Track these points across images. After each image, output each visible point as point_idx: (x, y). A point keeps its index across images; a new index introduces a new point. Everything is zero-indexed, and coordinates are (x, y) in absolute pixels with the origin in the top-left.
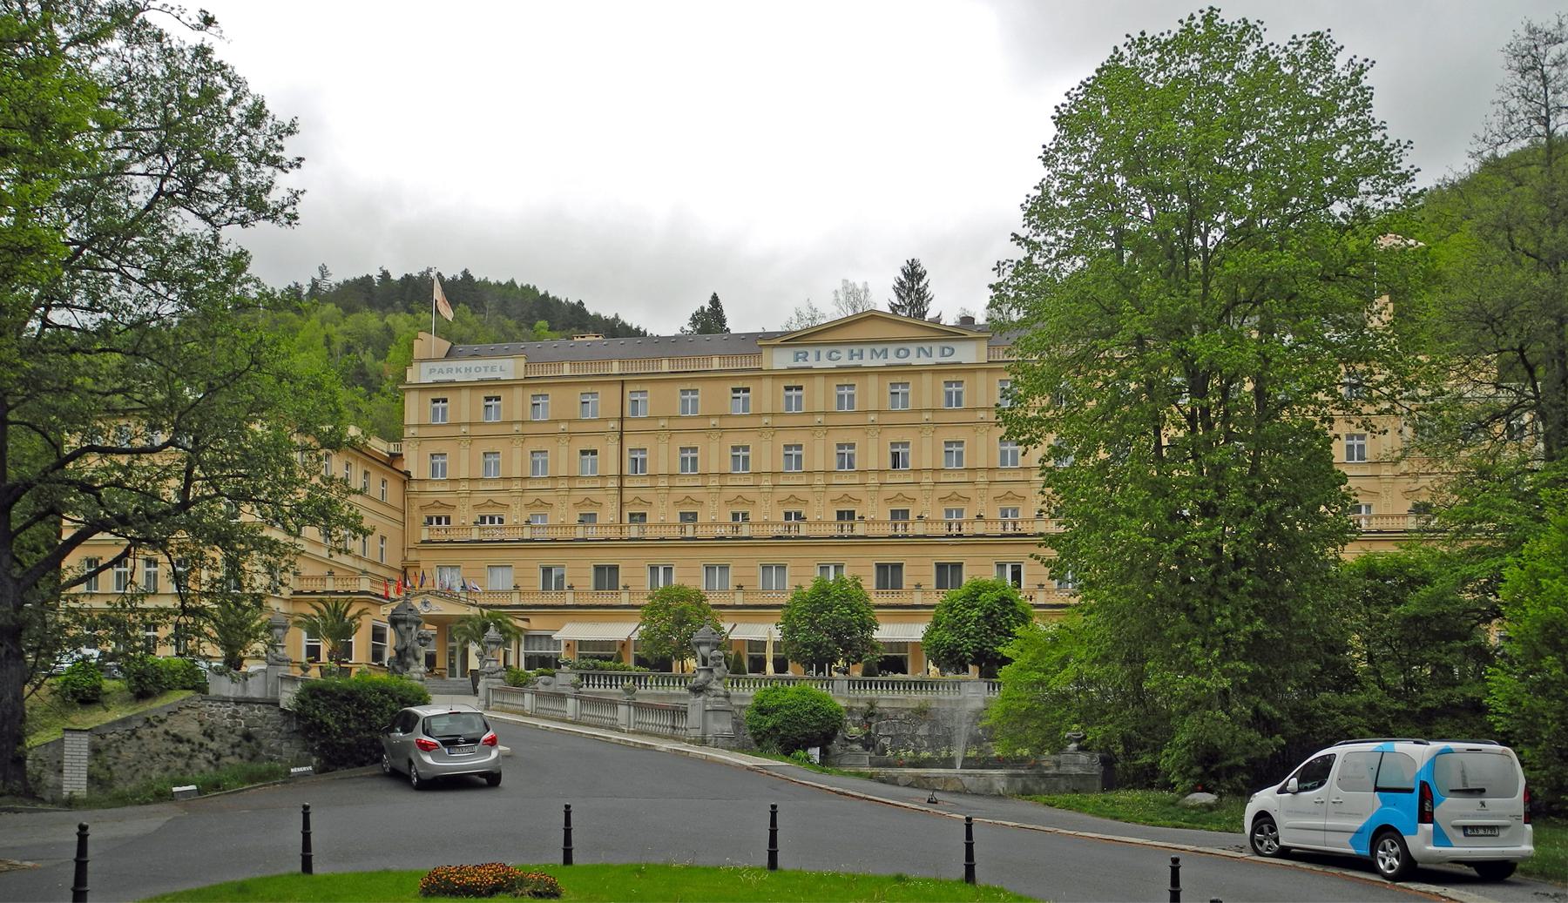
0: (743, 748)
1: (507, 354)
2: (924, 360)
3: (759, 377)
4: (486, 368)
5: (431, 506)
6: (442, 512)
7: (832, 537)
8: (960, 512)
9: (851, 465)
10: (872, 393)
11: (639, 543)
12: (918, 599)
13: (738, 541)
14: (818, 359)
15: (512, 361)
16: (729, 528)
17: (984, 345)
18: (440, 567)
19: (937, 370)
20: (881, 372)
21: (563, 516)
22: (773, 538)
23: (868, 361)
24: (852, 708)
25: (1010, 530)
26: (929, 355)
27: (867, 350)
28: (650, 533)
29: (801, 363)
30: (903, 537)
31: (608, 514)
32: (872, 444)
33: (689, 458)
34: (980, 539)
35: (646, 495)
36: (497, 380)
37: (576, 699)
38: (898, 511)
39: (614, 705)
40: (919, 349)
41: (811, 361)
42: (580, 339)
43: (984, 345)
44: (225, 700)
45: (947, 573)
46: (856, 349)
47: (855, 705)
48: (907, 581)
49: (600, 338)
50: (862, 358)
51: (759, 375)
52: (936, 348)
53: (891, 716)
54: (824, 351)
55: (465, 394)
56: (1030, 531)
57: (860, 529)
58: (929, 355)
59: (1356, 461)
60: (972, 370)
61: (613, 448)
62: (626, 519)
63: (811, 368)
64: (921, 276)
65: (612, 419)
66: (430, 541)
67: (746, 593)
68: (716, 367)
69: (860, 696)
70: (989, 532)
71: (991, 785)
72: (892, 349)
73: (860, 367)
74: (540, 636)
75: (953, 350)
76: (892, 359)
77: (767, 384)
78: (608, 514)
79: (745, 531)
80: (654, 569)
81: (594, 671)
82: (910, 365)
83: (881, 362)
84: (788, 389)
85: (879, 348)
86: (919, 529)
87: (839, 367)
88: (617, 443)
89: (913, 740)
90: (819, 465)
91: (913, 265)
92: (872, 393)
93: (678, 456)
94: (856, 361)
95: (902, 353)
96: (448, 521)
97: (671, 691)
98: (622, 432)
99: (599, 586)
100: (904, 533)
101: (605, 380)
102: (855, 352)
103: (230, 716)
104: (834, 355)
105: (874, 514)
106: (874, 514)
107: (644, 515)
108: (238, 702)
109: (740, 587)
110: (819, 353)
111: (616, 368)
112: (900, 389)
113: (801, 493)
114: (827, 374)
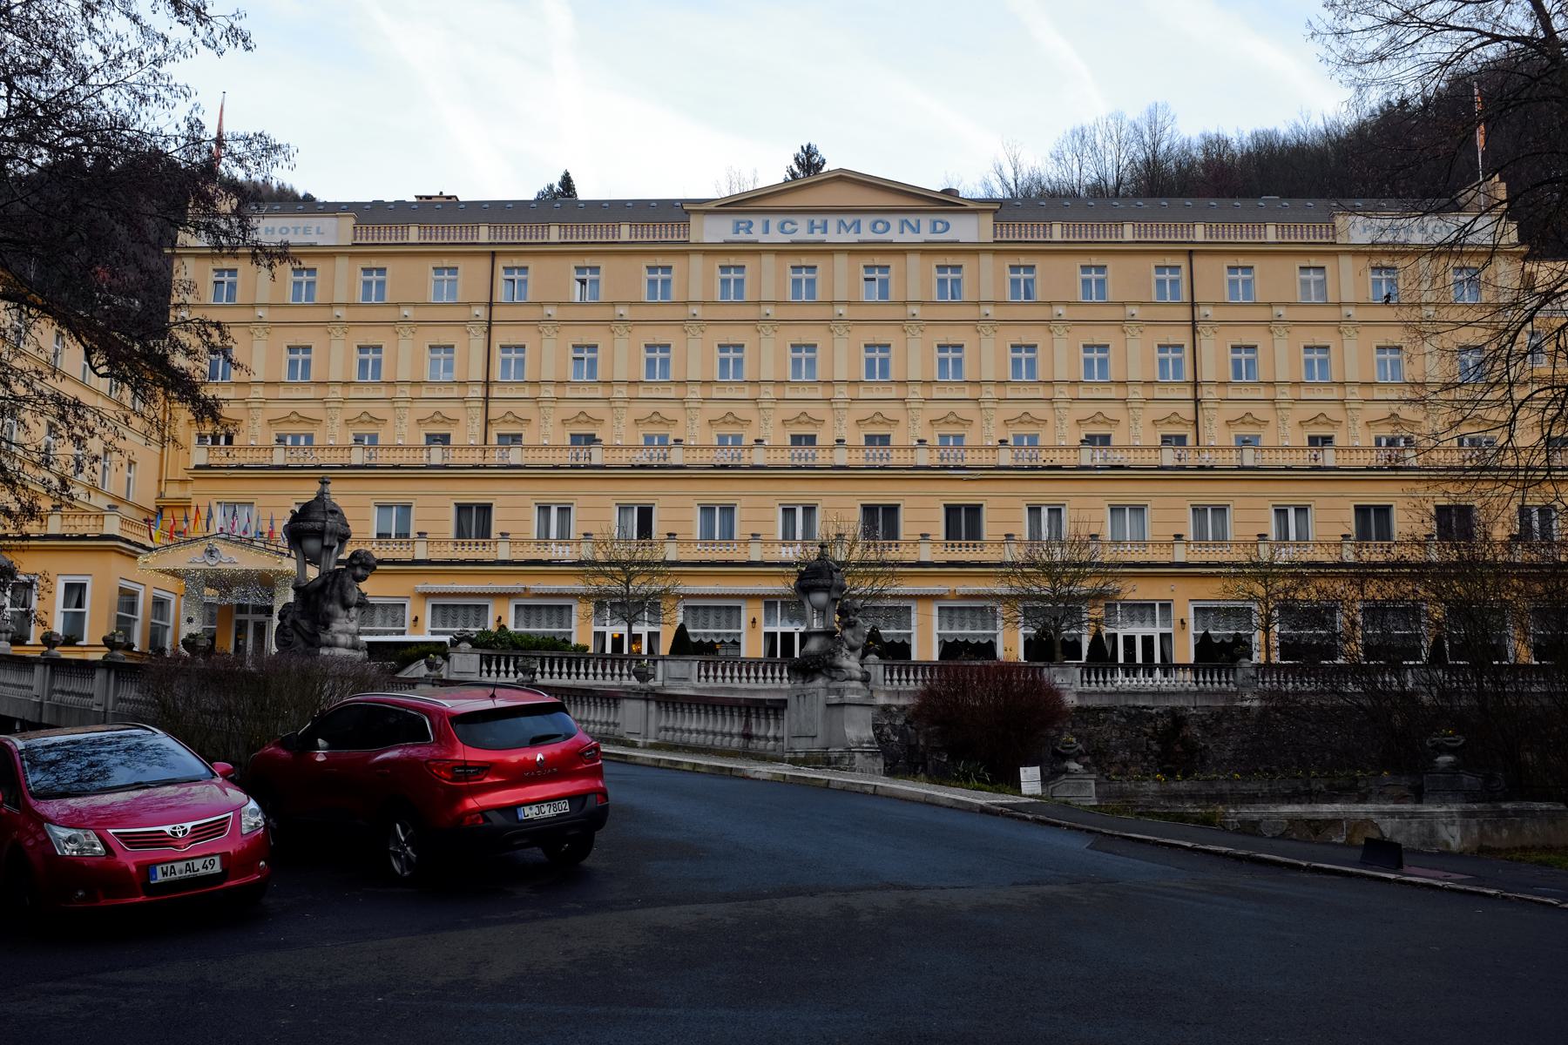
0: (891, 771)
3: (686, 253)
4: (296, 229)
5: (287, 420)
11: (445, 472)
12: (756, 553)
13: (1318, 473)
14: (767, 232)
15: (334, 220)
16: (479, 453)
20: (853, 250)
23: (833, 236)
24: (890, 706)
26: (917, 230)
27: (833, 221)
29: (743, 236)
31: (467, 432)
32: (549, 346)
33: (878, 355)
34: (758, 472)
35: (522, 409)
36: (311, 246)
37: (647, 700)
38: (875, 436)
39: (610, 699)
40: (902, 223)
41: (757, 234)
46: (818, 220)
47: (894, 701)
48: (906, 529)
51: (686, 250)
52: (925, 221)
54: (775, 221)
55: (768, 261)
57: (598, 457)
58: (917, 230)
59: (220, 380)
60: (974, 251)
61: (478, 344)
62: (493, 440)
63: (756, 243)
65: (478, 304)
66: (208, 467)
69: (901, 689)
71: (1433, 832)
72: (866, 221)
73: (823, 243)
75: (948, 224)
76: (867, 234)
77: (696, 262)
78: (467, 432)
79: (1329, 458)
80: (544, 509)
81: (555, 654)
82: (891, 243)
83: (851, 237)
85: (848, 219)
88: (484, 336)
91: (809, 151)
93: (356, 356)
94: (817, 235)
96: (229, 440)
98: (490, 321)
99: (952, 533)
104: (788, 227)
107: (448, 436)
110: (767, 222)
112: (588, 276)
113: (594, 409)
114: (780, 251)
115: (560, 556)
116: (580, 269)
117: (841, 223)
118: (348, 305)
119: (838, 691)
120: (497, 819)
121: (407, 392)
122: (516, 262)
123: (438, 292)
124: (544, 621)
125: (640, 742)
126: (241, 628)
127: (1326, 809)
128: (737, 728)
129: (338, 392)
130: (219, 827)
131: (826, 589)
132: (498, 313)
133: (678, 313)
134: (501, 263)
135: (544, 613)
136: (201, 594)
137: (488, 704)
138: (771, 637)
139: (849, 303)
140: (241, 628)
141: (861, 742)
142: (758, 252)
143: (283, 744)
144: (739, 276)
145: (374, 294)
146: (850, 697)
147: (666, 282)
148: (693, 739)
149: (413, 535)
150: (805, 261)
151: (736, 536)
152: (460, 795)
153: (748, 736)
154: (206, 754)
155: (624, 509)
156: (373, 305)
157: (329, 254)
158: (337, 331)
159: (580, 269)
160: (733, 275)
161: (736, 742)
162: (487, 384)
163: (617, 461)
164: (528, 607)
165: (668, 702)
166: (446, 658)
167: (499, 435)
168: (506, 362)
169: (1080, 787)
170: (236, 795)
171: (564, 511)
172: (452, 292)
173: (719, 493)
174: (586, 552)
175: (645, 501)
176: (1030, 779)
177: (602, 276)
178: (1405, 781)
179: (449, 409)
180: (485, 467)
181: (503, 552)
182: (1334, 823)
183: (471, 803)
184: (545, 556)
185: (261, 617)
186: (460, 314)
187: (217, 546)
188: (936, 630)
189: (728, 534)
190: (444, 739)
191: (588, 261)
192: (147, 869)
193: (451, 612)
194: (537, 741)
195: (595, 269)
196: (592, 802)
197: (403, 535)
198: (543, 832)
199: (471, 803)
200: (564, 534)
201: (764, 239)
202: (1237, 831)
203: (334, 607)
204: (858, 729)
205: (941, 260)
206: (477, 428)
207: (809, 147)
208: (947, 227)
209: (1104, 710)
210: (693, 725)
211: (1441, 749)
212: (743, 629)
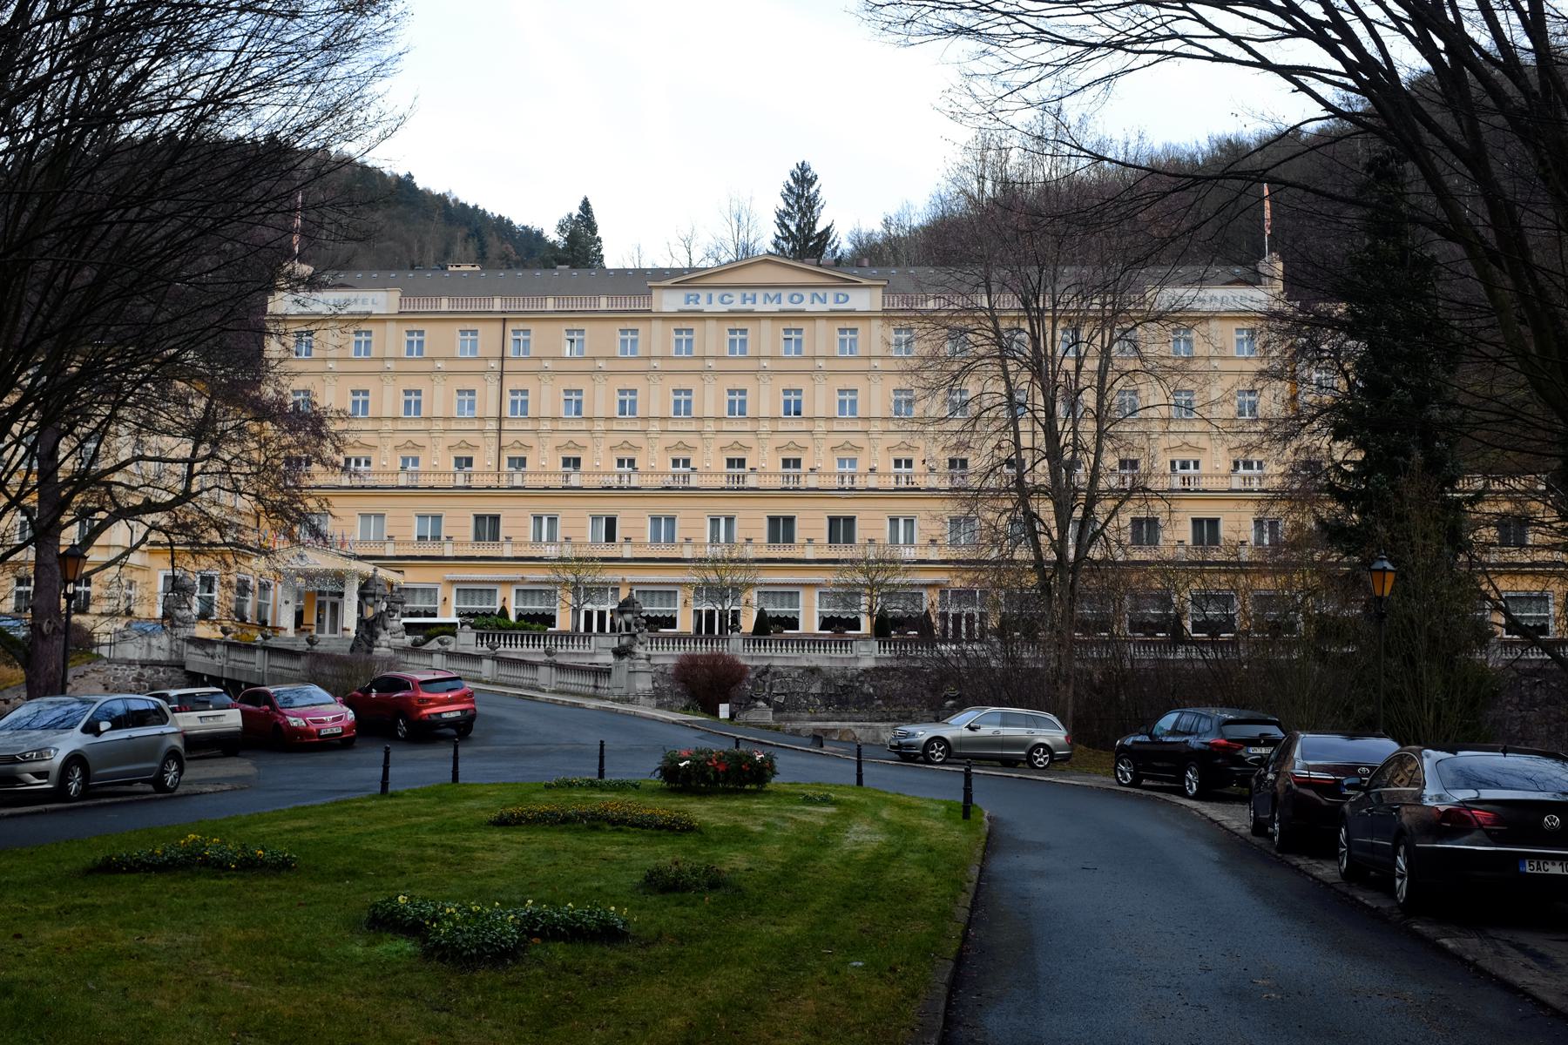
0: (660, 706)
1: (384, 286)
2: (818, 307)
6: (1190, 456)
7: (722, 489)
8: (853, 462)
9: (688, 412)
10: (766, 338)
12: (687, 553)
13: (569, 490)
14: (710, 303)
17: (879, 292)
18: (362, 515)
19: (832, 316)
20: (775, 317)
21: (437, 462)
22: (663, 489)
23: (760, 306)
25: (903, 484)
27: (760, 294)
28: (530, 481)
29: (692, 306)
30: (794, 489)
31: (485, 460)
35: (527, 439)
39: (534, 666)
41: (703, 305)
42: (454, 268)
43: (879, 292)
44: (130, 663)
45: (841, 528)
46: (749, 293)
48: (799, 535)
49: (477, 268)
50: (754, 302)
51: (648, 316)
52: (831, 294)
53: (785, 674)
54: (716, 294)
55: (711, 325)
56: (922, 485)
60: (866, 317)
61: (493, 388)
62: (505, 462)
64: (811, 182)
65: (493, 358)
67: (634, 545)
68: (603, 307)
70: (881, 485)
71: (878, 736)
72: (785, 294)
74: (414, 590)
76: (786, 305)
77: (657, 326)
79: (575, 480)
82: (803, 311)
83: (774, 307)
84: (732, 331)
85: (772, 293)
86: (812, 482)
87: (731, 311)
88: (497, 383)
89: (805, 698)
90: (709, 411)
91: (804, 168)
92: (766, 338)
94: (748, 306)
95: (796, 298)
97: (570, 650)
99: (833, 538)
100: (796, 485)
101: (487, 317)
102: (772, 296)
103: (135, 679)
104: (726, 299)
105: (765, 464)
106: (765, 464)
108: (143, 665)
109: (810, 540)
111: (497, 304)
114: (719, 318)
115: (548, 553)
116: (569, 331)
117: (767, 295)
118: (395, 359)
119: (633, 665)
120: (434, 718)
121: (441, 425)
122: (522, 326)
123: (463, 349)
124: (537, 601)
125: (547, 689)
126: (321, 606)
127: (831, 725)
128: (592, 683)
129: (389, 425)
130: (340, 718)
131: (631, 612)
132: (508, 365)
133: (643, 365)
134: (510, 327)
135: (537, 596)
136: (294, 583)
137: (432, 677)
138: (698, 613)
139: (771, 358)
140: (321, 606)
141: (644, 691)
142: (703, 319)
143: (360, 691)
144: (689, 337)
145: (416, 347)
146: (638, 668)
147: (634, 341)
148: (573, 688)
149: (443, 538)
150: (739, 325)
151: (677, 540)
152: (419, 709)
153: (596, 687)
154: (335, 694)
155: (595, 518)
156: (414, 359)
157: (382, 320)
158: (388, 379)
159: (569, 331)
160: (684, 336)
161: (591, 690)
162: (500, 419)
163: (591, 485)
164: (525, 591)
165: (562, 668)
166: (454, 635)
167: (509, 458)
168: (514, 403)
169: (763, 715)
170: (345, 708)
171: (552, 520)
172: (474, 349)
173: (664, 507)
174: (568, 552)
175: (611, 513)
176: (724, 710)
177: (586, 336)
178: (933, 714)
179: (472, 438)
180: (498, 488)
181: (507, 551)
182: (834, 730)
183: (425, 712)
184: (537, 554)
185: (335, 599)
186: (480, 366)
187: (305, 552)
188: (817, 609)
189: (671, 538)
190: (415, 689)
191: (576, 326)
192: (319, 731)
193: (470, 594)
194: (449, 690)
195: (581, 331)
196: (469, 713)
197: (436, 538)
198: (452, 723)
199: (425, 712)
200: (552, 538)
201: (708, 308)
202: (790, 734)
203: (380, 629)
204: (643, 684)
205: (842, 325)
206: (493, 453)
207: (803, 164)
208: (847, 298)
209: (894, 669)
210: (572, 680)
211: (947, 698)
212: (678, 608)
